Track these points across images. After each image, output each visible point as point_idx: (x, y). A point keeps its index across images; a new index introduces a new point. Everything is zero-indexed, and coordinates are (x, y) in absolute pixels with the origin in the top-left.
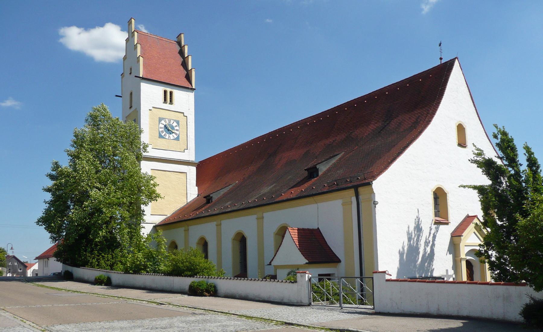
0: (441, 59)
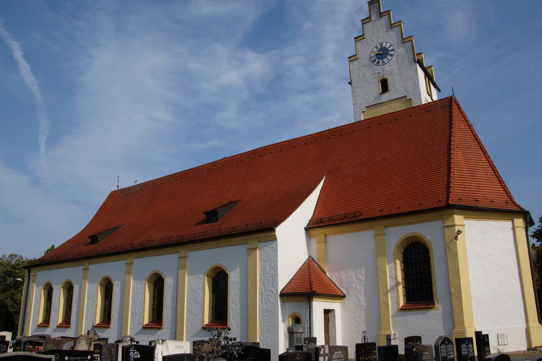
0: (118, 186)
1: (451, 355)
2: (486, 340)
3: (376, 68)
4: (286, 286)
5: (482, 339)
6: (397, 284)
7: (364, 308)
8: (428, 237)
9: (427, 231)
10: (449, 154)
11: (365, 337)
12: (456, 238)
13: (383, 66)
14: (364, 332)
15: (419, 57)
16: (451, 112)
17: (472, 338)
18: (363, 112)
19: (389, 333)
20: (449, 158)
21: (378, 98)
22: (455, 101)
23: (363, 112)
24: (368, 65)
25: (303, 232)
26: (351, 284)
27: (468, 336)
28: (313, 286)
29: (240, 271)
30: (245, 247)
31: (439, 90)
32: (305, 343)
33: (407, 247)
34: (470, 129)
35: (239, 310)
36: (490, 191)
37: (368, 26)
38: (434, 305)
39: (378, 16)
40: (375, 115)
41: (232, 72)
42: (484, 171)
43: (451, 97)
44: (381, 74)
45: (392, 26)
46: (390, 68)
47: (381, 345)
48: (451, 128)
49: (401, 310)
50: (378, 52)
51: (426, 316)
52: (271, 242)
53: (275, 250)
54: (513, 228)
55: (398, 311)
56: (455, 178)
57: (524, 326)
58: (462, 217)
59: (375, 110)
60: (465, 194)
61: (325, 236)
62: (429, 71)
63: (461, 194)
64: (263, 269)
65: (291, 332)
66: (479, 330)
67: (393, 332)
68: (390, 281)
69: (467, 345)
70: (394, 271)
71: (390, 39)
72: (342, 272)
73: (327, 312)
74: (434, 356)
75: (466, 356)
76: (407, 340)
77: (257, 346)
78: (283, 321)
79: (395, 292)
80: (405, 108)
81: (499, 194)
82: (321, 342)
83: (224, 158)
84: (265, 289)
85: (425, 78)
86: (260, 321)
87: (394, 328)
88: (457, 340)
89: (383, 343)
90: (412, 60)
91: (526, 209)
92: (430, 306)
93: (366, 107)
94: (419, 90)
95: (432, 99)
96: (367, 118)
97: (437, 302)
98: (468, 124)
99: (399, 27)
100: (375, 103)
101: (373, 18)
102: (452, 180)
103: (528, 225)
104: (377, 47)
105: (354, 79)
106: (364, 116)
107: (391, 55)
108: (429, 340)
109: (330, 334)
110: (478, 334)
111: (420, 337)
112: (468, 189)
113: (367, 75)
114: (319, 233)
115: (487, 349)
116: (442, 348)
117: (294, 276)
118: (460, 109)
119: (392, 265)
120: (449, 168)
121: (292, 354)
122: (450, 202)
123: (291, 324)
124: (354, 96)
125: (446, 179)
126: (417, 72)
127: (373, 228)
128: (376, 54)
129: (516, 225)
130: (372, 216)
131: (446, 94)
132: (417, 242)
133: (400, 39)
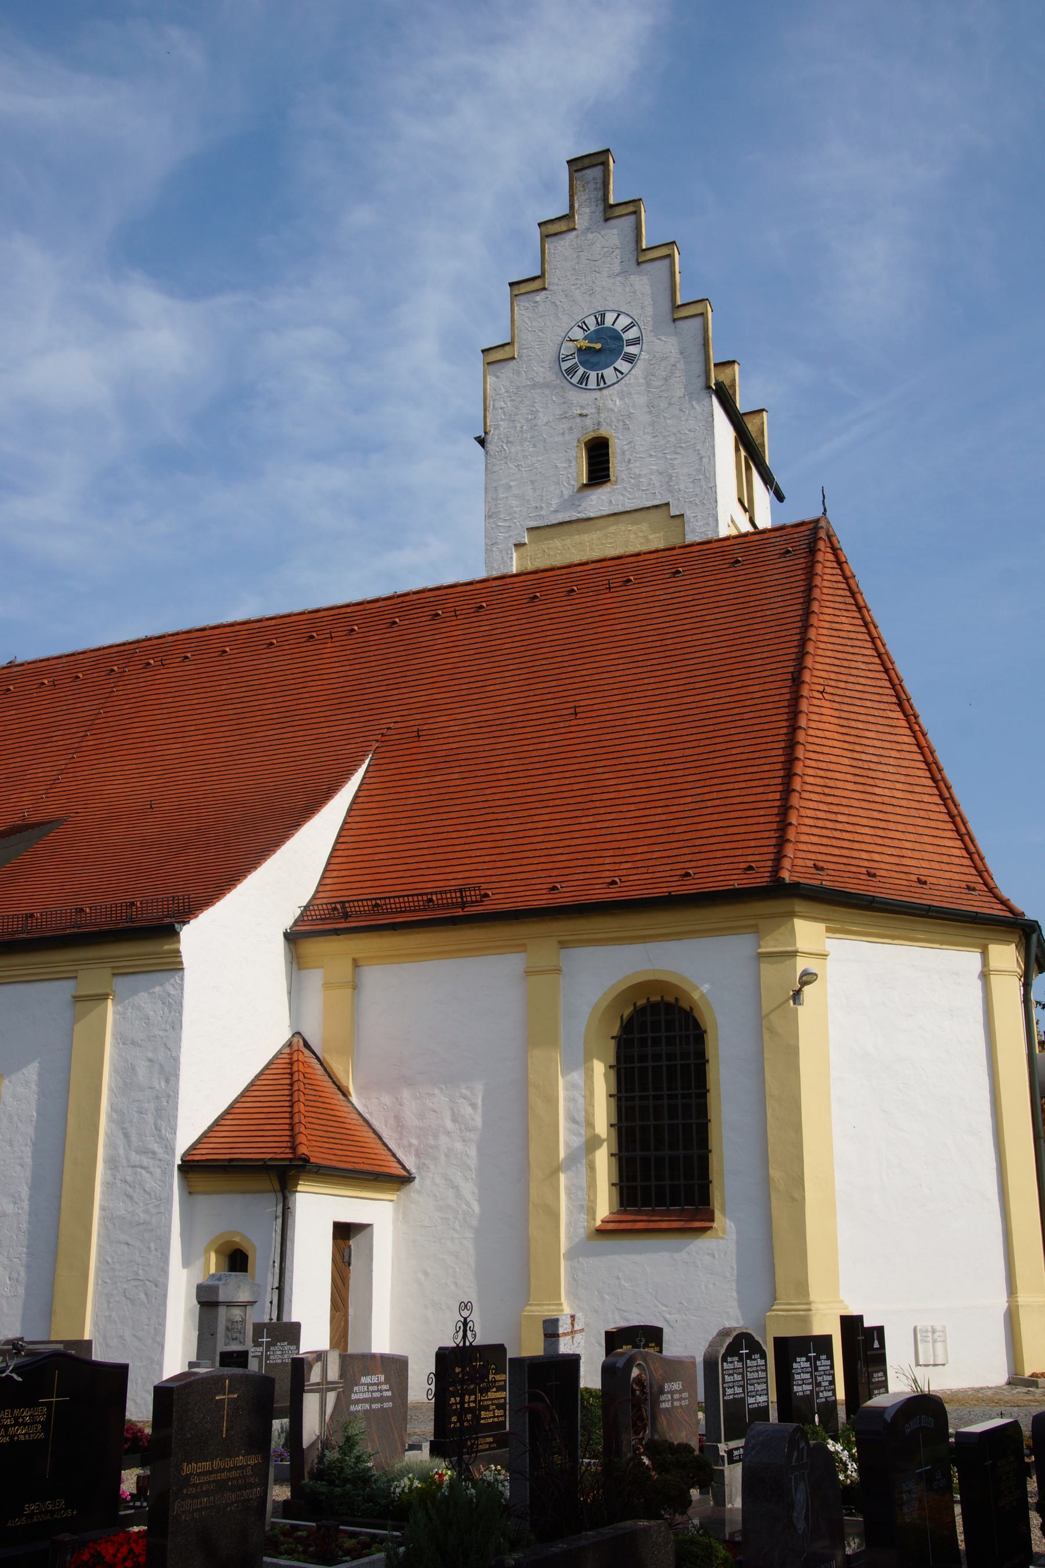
1: (758, 1393)
2: (876, 1345)
3: (575, 396)
4: (205, 1135)
5: (863, 1343)
6: (592, 1143)
7: (475, 1223)
8: (705, 988)
9: (701, 965)
10: (794, 713)
11: (465, 1323)
12: (797, 995)
13: (597, 394)
14: (465, 1306)
15: (724, 376)
16: (810, 573)
17: (828, 1339)
18: (519, 546)
19: (554, 1314)
20: (794, 728)
21: (571, 503)
22: (829, 537)
23: (519, 546)
24: (547, 385)
25: (279, 944)
26: (436, 1136)
27: (818, 1330)
28: (301, 1138)
29: (40, 1075)
30: (64, 990)
31: (779, 496)
32: (257, 1344)
33: (631, 1019)
34: (869, 633)
35: (24, 1218)
36: (917, 846)
37: (561, 247)
38: (713, 1220)
39: (599, 215)
40: (558, 561)
41: (94, 351)
42: (903, 779)
43: (817, 521)
44: (588, 421)
45: (641, 255)
46: (621, 404)
47: (525, 1354)
48: (806, 626)
49: (600, 1232)
50: (585, 344)
51: (683, 1255)
52: (159, 975)
53: (175, 1006)
54: (985, 976)
55: (589, 1237)
56: (805, 795)
57: (1001, 1303)
58: (822, 926)
59: (558, 543)
60: (837, 852)
61: (356, 963)
62: (751, 425)
63: (823, 849)
64: (126, 1072)
65: (208, 1301)
66: (854, 1311)
67: (567, 1310)
68: (570, 1131)
69: (813, 1362)
70: (584, 1099)
71: (630, 301)
72: (406, 1094)
73: (344, 1232)
74: (701, 1396)
75: (808, 1399)
76: (614, 1339)
77: (83, 1355)
78: (186, 1262)
79: (583, 1170)
80: (662, 546)
81: (945, 859)
82: (315, 1336)
83: (11, 665)
84: (129, 1142)
85: (737, 450)
86: (102, 1261)
87: (573, 1294)
88: (781, 1343)
89: (533, 1347)
90: (700, 382)
91: (1030, 915)
92: (697, 1224)
93: (530, 530)
94: (713, 489)
95: (752, 521)
96: (530, 567)
97: (723, 1211)
98: (863, 619)
99: (666, 262)
100: (561, 517)
101: (581, 221)
102: (795, 800)
103: (1034, 967)
104: (583, 326)
105: (497, 427)
106: (520, 558)
107: (630, 359)
108: (687, 1341)
109: (351, 1311)
110: (851, 1324)
111: (659, 1331)
112: (845, 835)
113: (542, 418)
114: (334, 953)
115: (877, 1377)
116: (730, 1370)
117: (236, 1101)
118: (840, 564)
119: (577, 1076)
120: (790, 760)
121: (205, 1380)
122: (786, 875)
123: (213, 1270)
124: (491, 489)
125: (778, 796)
126: (713, 427)
127: (521, 947)
128: (580, 350)
129: (993, 964)
130: (521, 906)
131: (801, 510)
132: (668, 1005)
133: (666, 306)
